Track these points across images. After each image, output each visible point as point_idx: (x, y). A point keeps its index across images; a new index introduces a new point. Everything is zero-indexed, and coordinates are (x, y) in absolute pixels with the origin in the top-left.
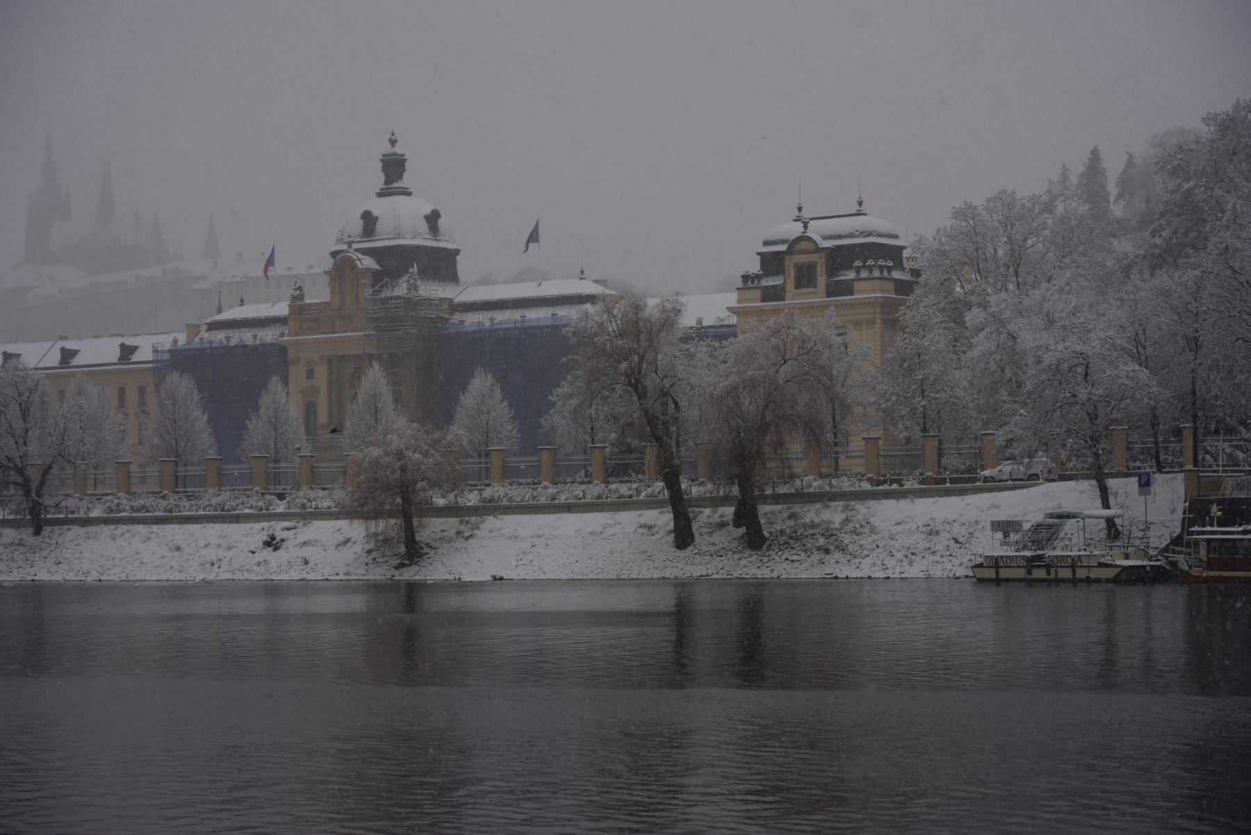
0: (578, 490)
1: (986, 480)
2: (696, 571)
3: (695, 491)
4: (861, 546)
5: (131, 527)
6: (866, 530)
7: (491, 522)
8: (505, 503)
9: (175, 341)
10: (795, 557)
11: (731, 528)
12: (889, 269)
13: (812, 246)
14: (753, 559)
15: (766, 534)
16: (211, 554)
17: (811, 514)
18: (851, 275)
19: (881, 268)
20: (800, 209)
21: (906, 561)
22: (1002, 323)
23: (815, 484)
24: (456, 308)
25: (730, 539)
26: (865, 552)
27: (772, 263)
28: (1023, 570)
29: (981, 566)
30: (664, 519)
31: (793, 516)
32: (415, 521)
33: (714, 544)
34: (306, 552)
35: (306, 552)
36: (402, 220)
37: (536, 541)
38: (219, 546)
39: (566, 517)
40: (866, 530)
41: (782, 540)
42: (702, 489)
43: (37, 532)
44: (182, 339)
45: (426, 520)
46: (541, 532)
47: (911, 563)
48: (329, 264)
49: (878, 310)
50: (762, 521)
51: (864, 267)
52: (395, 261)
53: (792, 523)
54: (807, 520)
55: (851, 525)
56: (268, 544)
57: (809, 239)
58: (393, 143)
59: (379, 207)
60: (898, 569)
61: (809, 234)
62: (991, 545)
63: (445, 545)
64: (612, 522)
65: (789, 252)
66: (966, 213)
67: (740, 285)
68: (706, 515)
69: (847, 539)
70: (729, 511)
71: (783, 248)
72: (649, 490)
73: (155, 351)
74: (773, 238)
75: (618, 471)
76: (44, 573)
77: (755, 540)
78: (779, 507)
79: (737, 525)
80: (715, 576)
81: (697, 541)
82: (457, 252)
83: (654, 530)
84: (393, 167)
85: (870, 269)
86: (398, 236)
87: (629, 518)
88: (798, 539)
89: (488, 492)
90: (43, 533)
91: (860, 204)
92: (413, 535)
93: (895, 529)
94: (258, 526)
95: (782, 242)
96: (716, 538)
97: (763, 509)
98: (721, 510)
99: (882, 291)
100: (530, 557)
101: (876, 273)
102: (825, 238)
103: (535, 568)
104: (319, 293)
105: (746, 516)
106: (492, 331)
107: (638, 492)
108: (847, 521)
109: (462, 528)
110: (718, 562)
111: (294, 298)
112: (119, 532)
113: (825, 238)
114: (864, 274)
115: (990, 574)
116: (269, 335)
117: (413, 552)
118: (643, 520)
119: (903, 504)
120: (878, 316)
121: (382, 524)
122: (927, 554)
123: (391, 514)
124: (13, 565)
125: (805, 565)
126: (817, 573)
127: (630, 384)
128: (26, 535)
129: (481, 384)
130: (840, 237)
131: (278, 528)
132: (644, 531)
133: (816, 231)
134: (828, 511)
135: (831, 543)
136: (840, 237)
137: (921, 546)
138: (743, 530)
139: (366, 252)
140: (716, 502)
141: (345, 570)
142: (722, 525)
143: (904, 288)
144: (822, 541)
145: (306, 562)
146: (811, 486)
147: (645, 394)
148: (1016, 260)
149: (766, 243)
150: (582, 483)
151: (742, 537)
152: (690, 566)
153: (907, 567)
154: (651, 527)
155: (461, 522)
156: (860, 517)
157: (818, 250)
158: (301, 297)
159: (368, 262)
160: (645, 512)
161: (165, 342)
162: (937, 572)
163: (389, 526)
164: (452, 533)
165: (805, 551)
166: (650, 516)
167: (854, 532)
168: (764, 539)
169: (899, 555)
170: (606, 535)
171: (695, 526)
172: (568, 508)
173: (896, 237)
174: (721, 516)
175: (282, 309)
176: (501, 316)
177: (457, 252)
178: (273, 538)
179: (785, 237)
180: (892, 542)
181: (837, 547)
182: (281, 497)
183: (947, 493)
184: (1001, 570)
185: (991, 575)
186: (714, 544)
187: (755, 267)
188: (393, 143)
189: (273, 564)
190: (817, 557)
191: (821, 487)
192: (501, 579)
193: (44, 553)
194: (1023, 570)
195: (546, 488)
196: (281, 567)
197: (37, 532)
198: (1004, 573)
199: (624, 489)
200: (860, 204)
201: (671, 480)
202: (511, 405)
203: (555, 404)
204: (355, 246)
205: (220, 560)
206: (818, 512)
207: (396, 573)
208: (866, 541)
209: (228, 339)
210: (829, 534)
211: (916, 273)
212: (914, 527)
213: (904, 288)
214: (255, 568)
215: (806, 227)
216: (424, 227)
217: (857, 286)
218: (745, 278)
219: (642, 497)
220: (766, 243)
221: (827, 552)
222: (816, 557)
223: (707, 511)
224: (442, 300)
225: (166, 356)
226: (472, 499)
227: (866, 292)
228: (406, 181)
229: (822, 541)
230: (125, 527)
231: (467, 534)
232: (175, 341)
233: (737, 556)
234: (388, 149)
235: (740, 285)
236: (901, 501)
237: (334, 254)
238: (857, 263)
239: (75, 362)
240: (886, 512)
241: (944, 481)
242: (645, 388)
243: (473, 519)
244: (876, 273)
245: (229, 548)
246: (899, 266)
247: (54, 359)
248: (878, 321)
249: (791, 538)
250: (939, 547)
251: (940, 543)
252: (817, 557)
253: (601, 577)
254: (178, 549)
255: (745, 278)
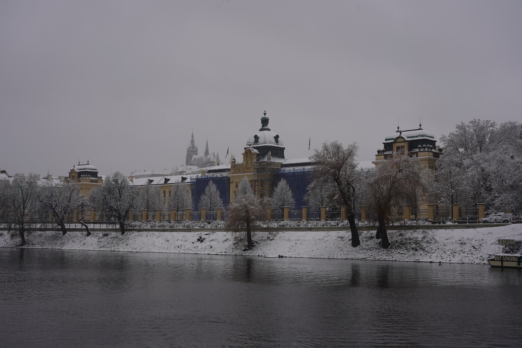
0: (315, 222)
1: (485, 222)
2: (361, 256)
3: (360, 224)
4: (431, 248)
5: (154, 232)
6: (433, 242)
7: (281, 234)
8: (288, 226)
9: (197, 176)
10: (402, 252)
11: (375, 239)
12: (431, 148)
13: (403, 140)
14: (384, 252)
15: (390, 242)
16: (178, 243)
17: (409, 234)
18: (417, 150)
19: (428, 148)
20: (398, 128)
21: (451, 256)
22: (479, 164)
23: (408, 223)
24: (283, 166)
25: (375, 243)
26: (433, 251)
27: (388, 146)
28: (516, 263)
29: (493, 260)
30: (348, 234)
31: (401, 235)
32: (252, 233)
33: (368, 245)
34: (212, 243)
35: (212, 243)
36: (267, 138)
37: (297, 242)
38: (182, 240)
39: (309, 233)
40: (433, 242)
41: (397, 244)
42: (363, 223)
43: (123, 234)
44: (200, 175)
45: (256, 233)
46: (299, 238)
47: (454, 256)
48: (244, 151)
49: (427, 162)
50: (388, 237)
51: (422, 147)
52: (264, 150)
53: (400, 238)
54: (407, 237)
55: (426, 239)
56: (199, 240)
57: (402, 138)
58: (265, 114)
59: (260, 134)
60: (448, 259)
61: (402, 136)
62: (498, 251)
63: (263, 242)
64: (327, 235)
65: (395, 142)
66: (462, 128)
67: (377, 154)
68: (364, 234)
69: (425, 245)
70: (374, 232)
71: (393, 141)
72: (343, 223)
73: (191, 179)
74: (388, 138)
75: (333, 215)
76: (122, 248)
77: (385, 244)
78: (395, 231)
79: (378, 237)
80: (368, 259)
81: (361, 244)
82: (284, 149)
83: (344, 239)
84: (265, 121)
85: (424, 148)
86: (265, 143)
87: (334, 234)
88: (403, 244)
89: (282, 223)
90: (125, 234)
91: (420, 126)
92: (251, 239)
93: (446, 242)
94: (197, 233)
95: (392, 139)
96: (369, 243)
97: (389, 232)
98: (371, 232)
99: (429, 156)
100: (294, 248)
101: (426, 149)
102: (408, 137)
103: (296, 253)
104: (240, 160)
105: (382, 234)
106: (294, 173)
107: (338, 225)
108: (424, 237)
109: (270, 236)
110: (369, 255)
111: (233, 162)
112: (149, 234)
113: (408, 137)
114: (422, 150)
115: (499, 264)
116: (225, 174)
117: (251, 245)
118: (340, 235)
119: (448, 231)
120: (427, 165)
121: (238, 234)
122: (461, 253)
123: (241, 230)
124: (113, 245)
125: (407, 255)
126: (412, 259)
127: (335, 180)
128: (119, 234)
129: (283, 183)
130: (413, 137)
131: (203, 234)
132: (340, 239)
133: (404, 135)
134: (416, 233)
135: (418, 246)
136: (413, 137)
137: (459, 249)
138: (380, 240)
139: (255, 148)
140: (369, 228)
141: (224, 251)
142: (371, 238)
143: (436, 155)
144: (414, 246)
145: (211, 247)
146: (407, 223)
147: (341, 184)
148: (481, 143)
149: (386, 140)
150: (316, 220)
151: (380, 243)
152: (358, 254)
153: (452, 258)
154: (342, 238)
155: (270, 234)
156: (430, 236)
157: (405, 141)
158: (235, 162)
159: (256, 151)
160: (340, 232)
161: (194, 176)
162: (466, 260)
163: (243, 234)
164: (266, 238)
165: (407, 249)
166: (342, 233)
167: (428, 242)
168: (389, 244)
169: (448, 253)
170: (324, 240)
171: (360, 238)
172: (310, 229)
173: (433, 138)
174: (371, 234)
175: (229, 167)
176: (297, 168)
177: (284, 149)
178: (201, 238)
179: (393, 137)
180: (445, 247)
181: (421, 248)
182: (209, 223)
183: (468, 227)
184: (504, 262)
185: (498, 266)
186: (368, 245)
187: (382, 148)
188: (265, 114)
189: (200, 248)
190: (412, 252)
191: (411, 224)
192: (282, 257)
193: (123, 241)
194: (516, 263)
195: (303, 222)
196: (203, 249)
197: (123, 234)
198: (505, 264)
199: (333, 223)
200: (420, 126)
201: (351, 218)
202: (292, 192)
203: (308, 190)
204: (252, 146)
205: (181, 245)
206: (412, 234)
207: (243, 252)
208: (433, 246)
209: (213, 175)
210: (417, 242)
211: (441, 150)
212: (454, 241)
213: (436, 155)
214: (193, 249)
215: (401, 133)
216: (274, 140)
217: (419, 154)
218: (379, 152)
219: (340, 226)
220: (386, 140)
221: (416, 250)
222: (411, 252)
223: (365, 232)
224: (278, 163)
225: (195, 181)
226: (275, 225)
227: (423, 156)
228: (269, 126)
229: (414, 246)
230: (152, 232)
231: (271, 238)
232: (197, 176)
233: (377, 251)
234: (263, 116)
235: (377, 154)
236: (448, 230)
237: (245, 148)
238: (419, 146)
239: (169, 182)
240: (440, 234)
241: (466, 223)
242: (341, 182)
243: (274, 233)
244: (426, 149)
245: (185, 241)
246: (434, 147)
247: (163, 181)
248: (427, 166)
249: (400, 244)
250: (466, 250)
251: (467, 248)
252: (412, 252)
253: (322, 257)
254: (168, 241)
255: (379, 152)
